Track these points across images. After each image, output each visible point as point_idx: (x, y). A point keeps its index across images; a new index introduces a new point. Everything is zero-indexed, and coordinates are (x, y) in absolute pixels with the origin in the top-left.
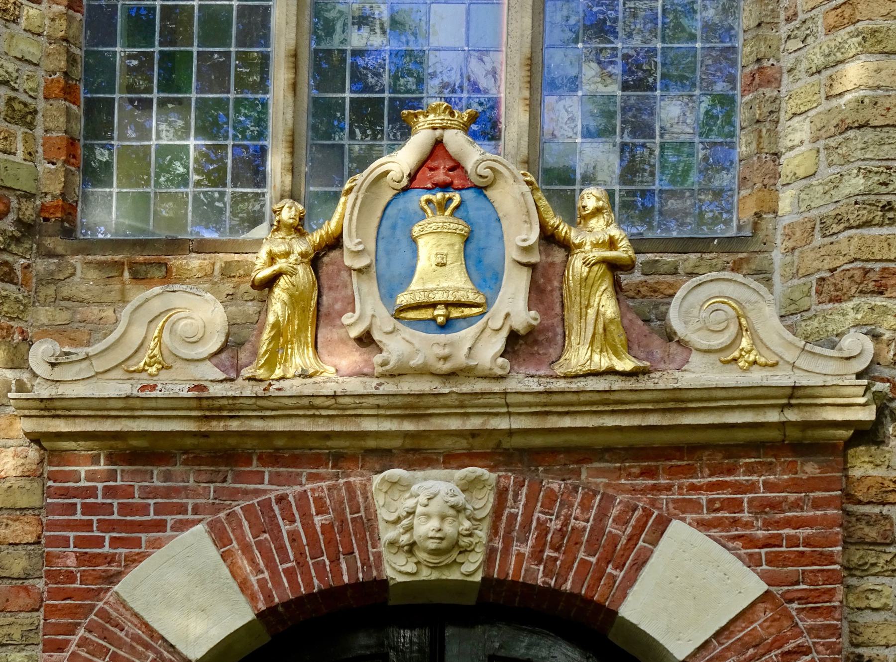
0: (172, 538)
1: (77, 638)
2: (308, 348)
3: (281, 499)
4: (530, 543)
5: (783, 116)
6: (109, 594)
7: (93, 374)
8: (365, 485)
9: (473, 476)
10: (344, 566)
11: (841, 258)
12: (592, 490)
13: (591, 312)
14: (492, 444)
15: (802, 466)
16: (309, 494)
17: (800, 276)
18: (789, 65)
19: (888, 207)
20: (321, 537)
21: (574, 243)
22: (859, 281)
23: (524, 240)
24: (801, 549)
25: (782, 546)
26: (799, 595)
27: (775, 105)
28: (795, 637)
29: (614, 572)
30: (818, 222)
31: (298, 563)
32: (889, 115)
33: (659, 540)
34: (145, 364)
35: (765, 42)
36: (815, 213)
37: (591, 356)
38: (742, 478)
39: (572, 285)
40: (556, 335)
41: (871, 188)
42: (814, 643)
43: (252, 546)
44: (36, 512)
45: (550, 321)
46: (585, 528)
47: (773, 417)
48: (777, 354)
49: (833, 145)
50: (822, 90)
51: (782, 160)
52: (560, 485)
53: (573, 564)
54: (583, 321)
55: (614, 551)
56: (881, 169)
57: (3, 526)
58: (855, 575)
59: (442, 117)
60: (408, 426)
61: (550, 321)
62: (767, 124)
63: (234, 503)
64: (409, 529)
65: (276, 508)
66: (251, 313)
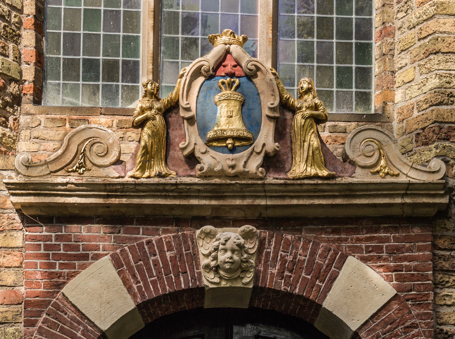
0: (91, 264)
1: (42, 319)
2: (162, 161)
3: (149, 242)
4: (277, 268)
5: (396, 52)
6: (59, 294)
7: (49, 172)
8: (192, 235)
9: (248, 230)
10: (182, 279)
11: (428, 122)
12: (308, 240)
13: (306, 144)
14: (257, 215)
15: (412, 229)
16: (163, 239)
17: (406, 133)
18: (399, 26)
19: (450, 95)
20: (170, 263)
21: (297, 107)
22: (437, 133)
23: (272, 104)
24: (412, 272)
25: (403, 271)
26: (412, 297)
27: (393, 47)
28: (411, 319)
29: (320, 284)
30: (415, 105)
31: (158, 278)
32: (450, 47)
33: (342, 267)
34: (77, 167)
35: (387, 14)
36: (413, 100)
37: (306, 168)
38: (382, 235)
39: (296, 129)
40: (288, 158)
41: (442, 84)
42: (420, 322)
43: (134, 268)
44: (20, 249)
45: (285, 150)
46: (305, 260)
47: (398, 200)
48: (398, 170)
49: (422, 63)
50: (416, 36)
51: (396, 75)
52: (292, 237)
53: (299, 279)
54: (302, 149)
55: (320, 273)
56: (447, 75)
57: (2, 257)
58: (438, 288)
59: (229, 38)
60: (214, 202)
61: (285, 150)
62: (389, 56)
63: (124, 245)
64: (215, 258)
65: (146, 247)
66: (132, 148)
